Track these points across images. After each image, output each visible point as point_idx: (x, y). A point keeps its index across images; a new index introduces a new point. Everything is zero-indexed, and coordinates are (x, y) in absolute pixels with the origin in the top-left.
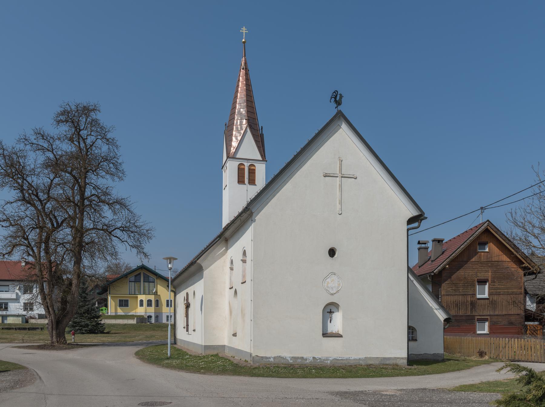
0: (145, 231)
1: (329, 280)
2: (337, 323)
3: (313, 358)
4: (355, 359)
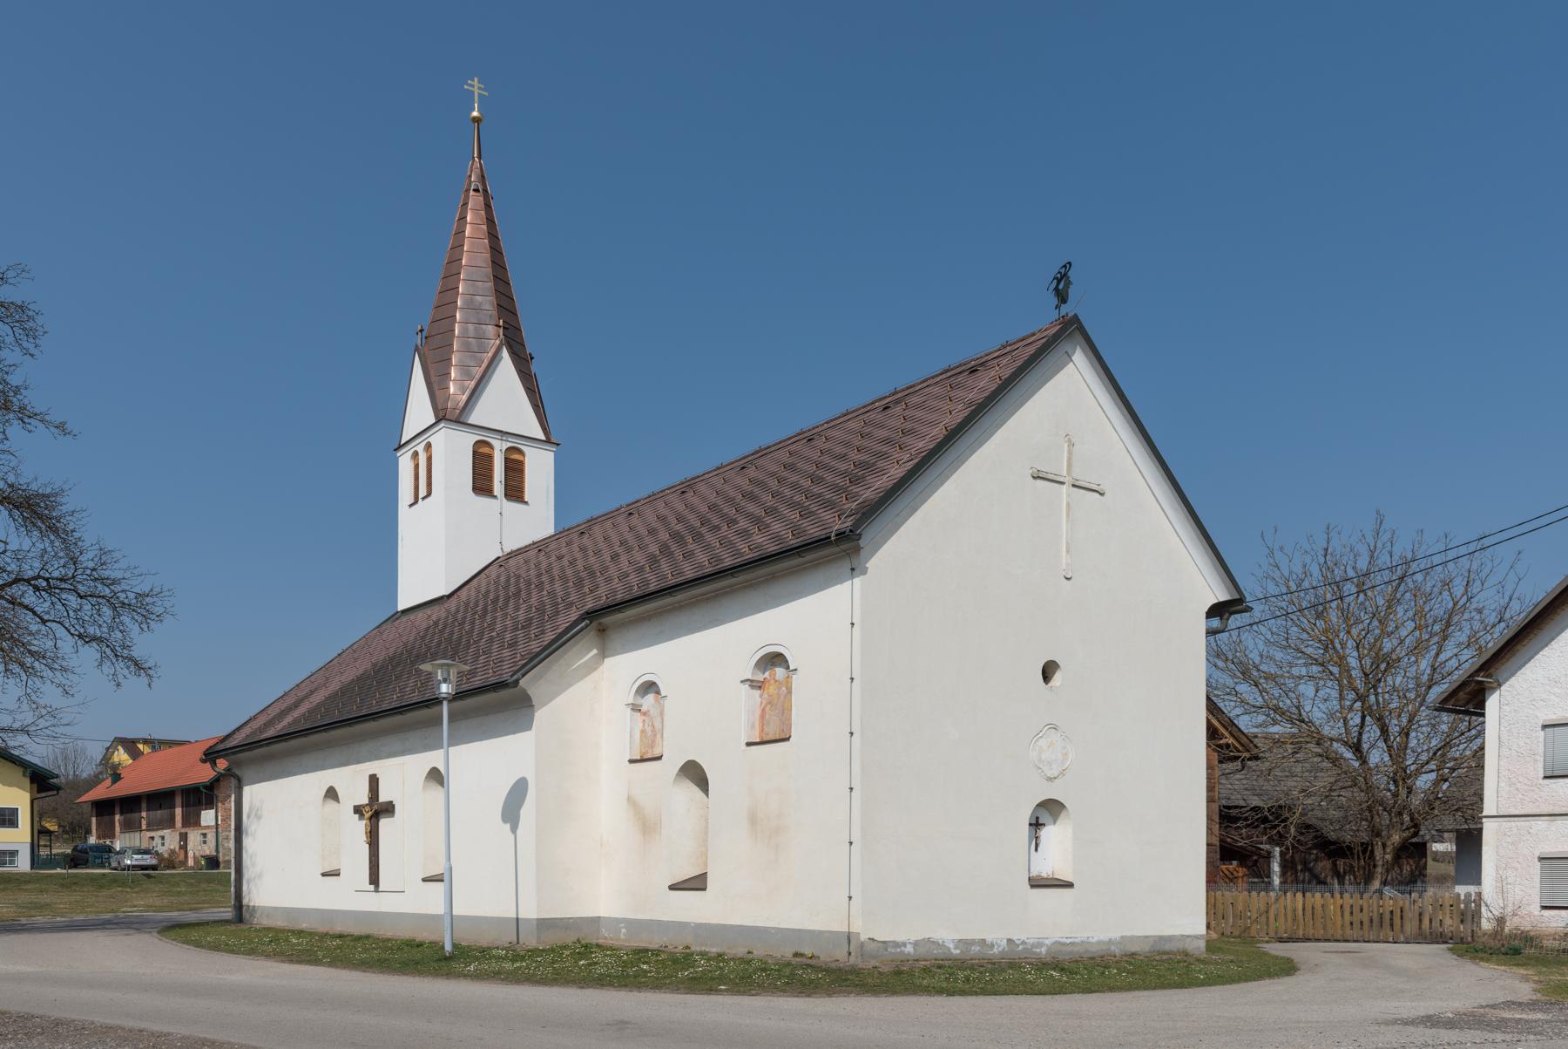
0: (132, 596)
1: (1043, 743)
2: (1057, 850)
3: (1009, 941)
4: (1099, 942)
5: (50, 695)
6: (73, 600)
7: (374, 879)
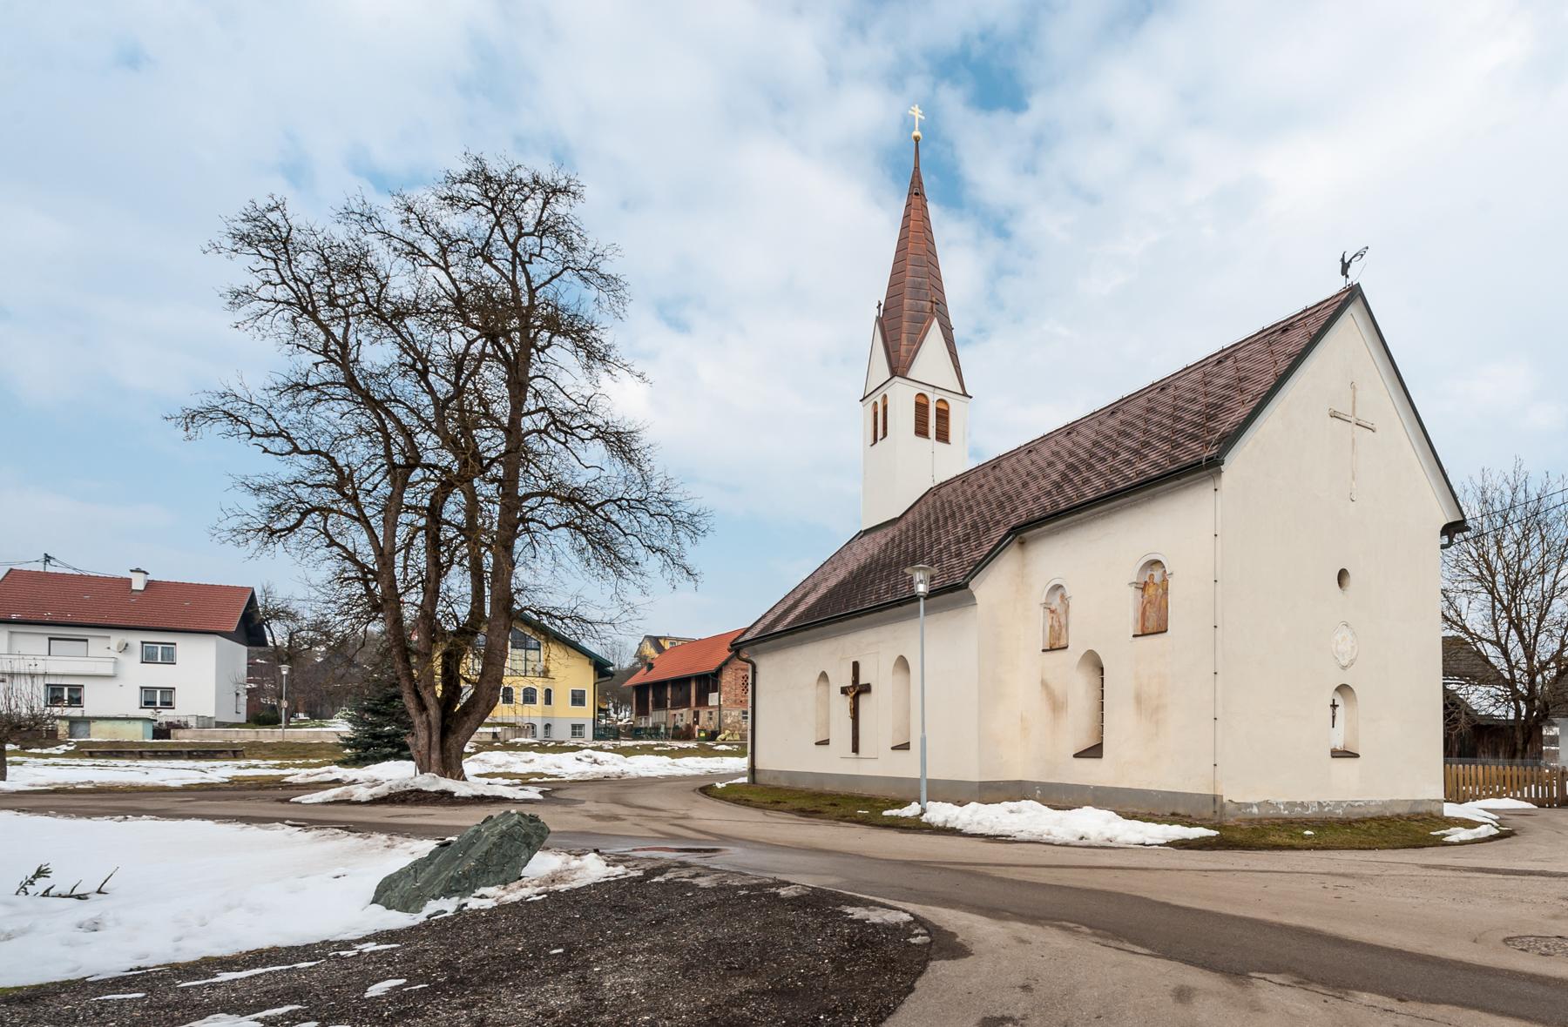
5: (632, 594)
6: (646, 519)
7: (856, 749)
